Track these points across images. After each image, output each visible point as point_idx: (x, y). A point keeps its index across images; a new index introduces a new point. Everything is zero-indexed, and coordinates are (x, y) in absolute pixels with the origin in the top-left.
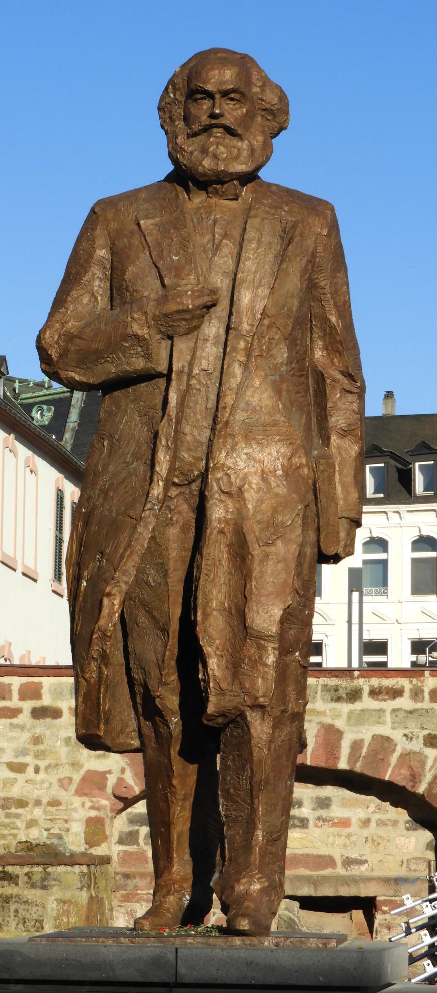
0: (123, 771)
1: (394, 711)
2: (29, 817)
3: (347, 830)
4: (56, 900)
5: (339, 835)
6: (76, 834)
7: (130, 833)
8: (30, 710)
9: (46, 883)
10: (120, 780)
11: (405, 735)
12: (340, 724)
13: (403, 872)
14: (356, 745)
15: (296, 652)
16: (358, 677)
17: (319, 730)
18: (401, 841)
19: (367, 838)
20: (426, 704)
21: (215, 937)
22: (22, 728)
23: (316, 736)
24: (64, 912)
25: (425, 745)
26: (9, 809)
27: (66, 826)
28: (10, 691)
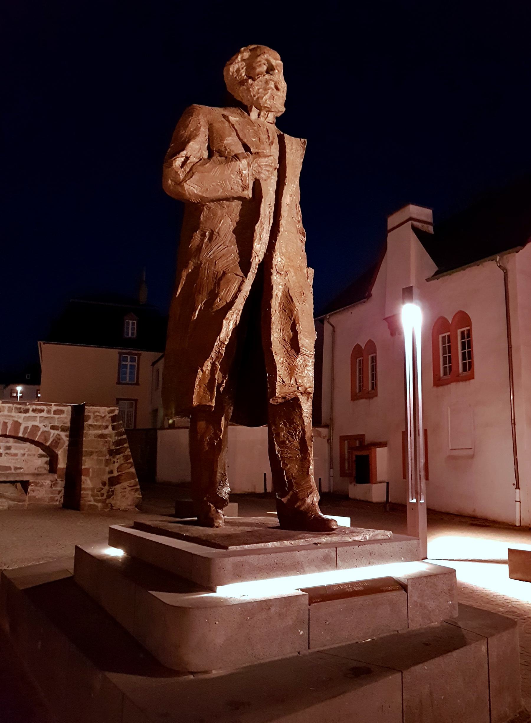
1: (40, 417)
3: (16, 457)
5: (13, 459)
11: (44, 425)
12: (20, 421)
13: (36, 472)
14: (26, 428)
15: (268, 390)
16: (28, 405)
17: (12, 423)
18: (36, 461)
19: (23, 460)
20: (52, 415)
23: (11, 425)
25: (51, 429)
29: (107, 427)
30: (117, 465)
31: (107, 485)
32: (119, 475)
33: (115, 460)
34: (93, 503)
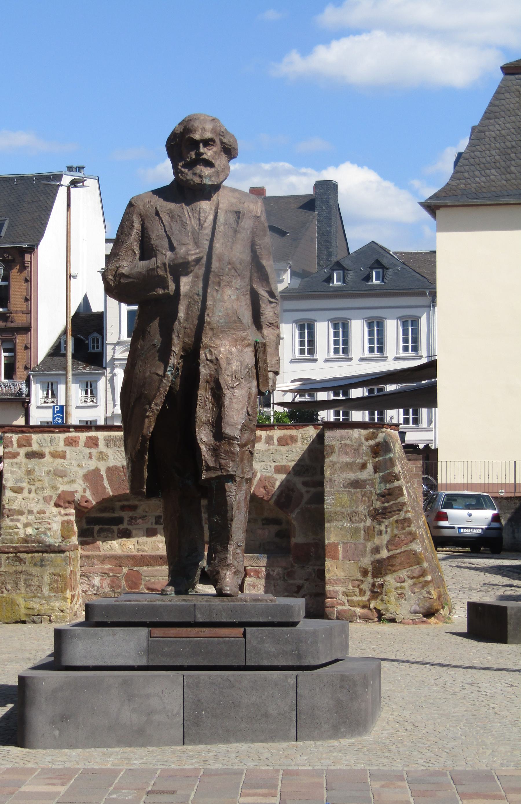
0: (84, 491)
2: (25, 521)
4: (50, 573)
6: (56, 532)
7: (88, 529)
8: (24, 453)
9: (43, 563)
10: (83, 497)
21: (360, 622)
22: (19, 465)
24: (54, 581)
26: (13, 516)
27: (49, 526)
28: (11, 442)
29: (364, 466)
30: (385, 538)
31: (370, 575)
32: (389, 558)
33: (383, 528)
34: (346, 607)
